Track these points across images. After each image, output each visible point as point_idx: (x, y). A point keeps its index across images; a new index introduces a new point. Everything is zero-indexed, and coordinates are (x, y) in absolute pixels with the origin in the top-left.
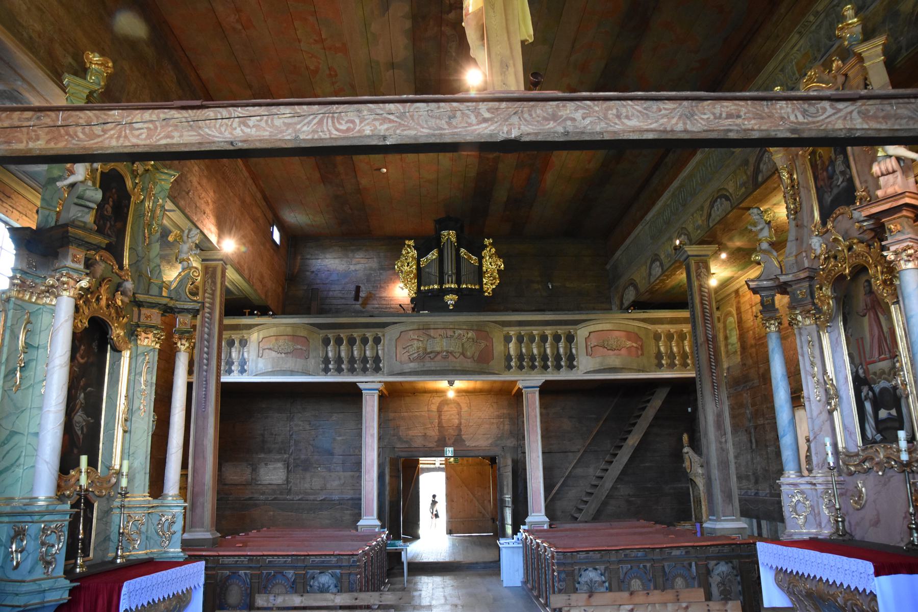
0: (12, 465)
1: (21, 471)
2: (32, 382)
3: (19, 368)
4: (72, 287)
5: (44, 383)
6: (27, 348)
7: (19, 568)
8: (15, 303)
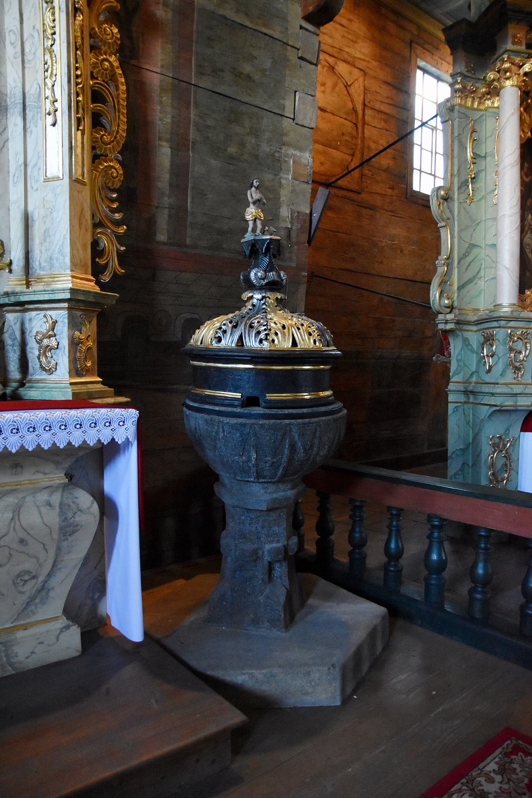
0: (474, 277)
1: (483, 283)
2: (483, 193)
3: (470, 180)
4: (516, 74)
5: (496, 192)
6: (475, 159)
7: (491, 372)
8: (459, 112)
